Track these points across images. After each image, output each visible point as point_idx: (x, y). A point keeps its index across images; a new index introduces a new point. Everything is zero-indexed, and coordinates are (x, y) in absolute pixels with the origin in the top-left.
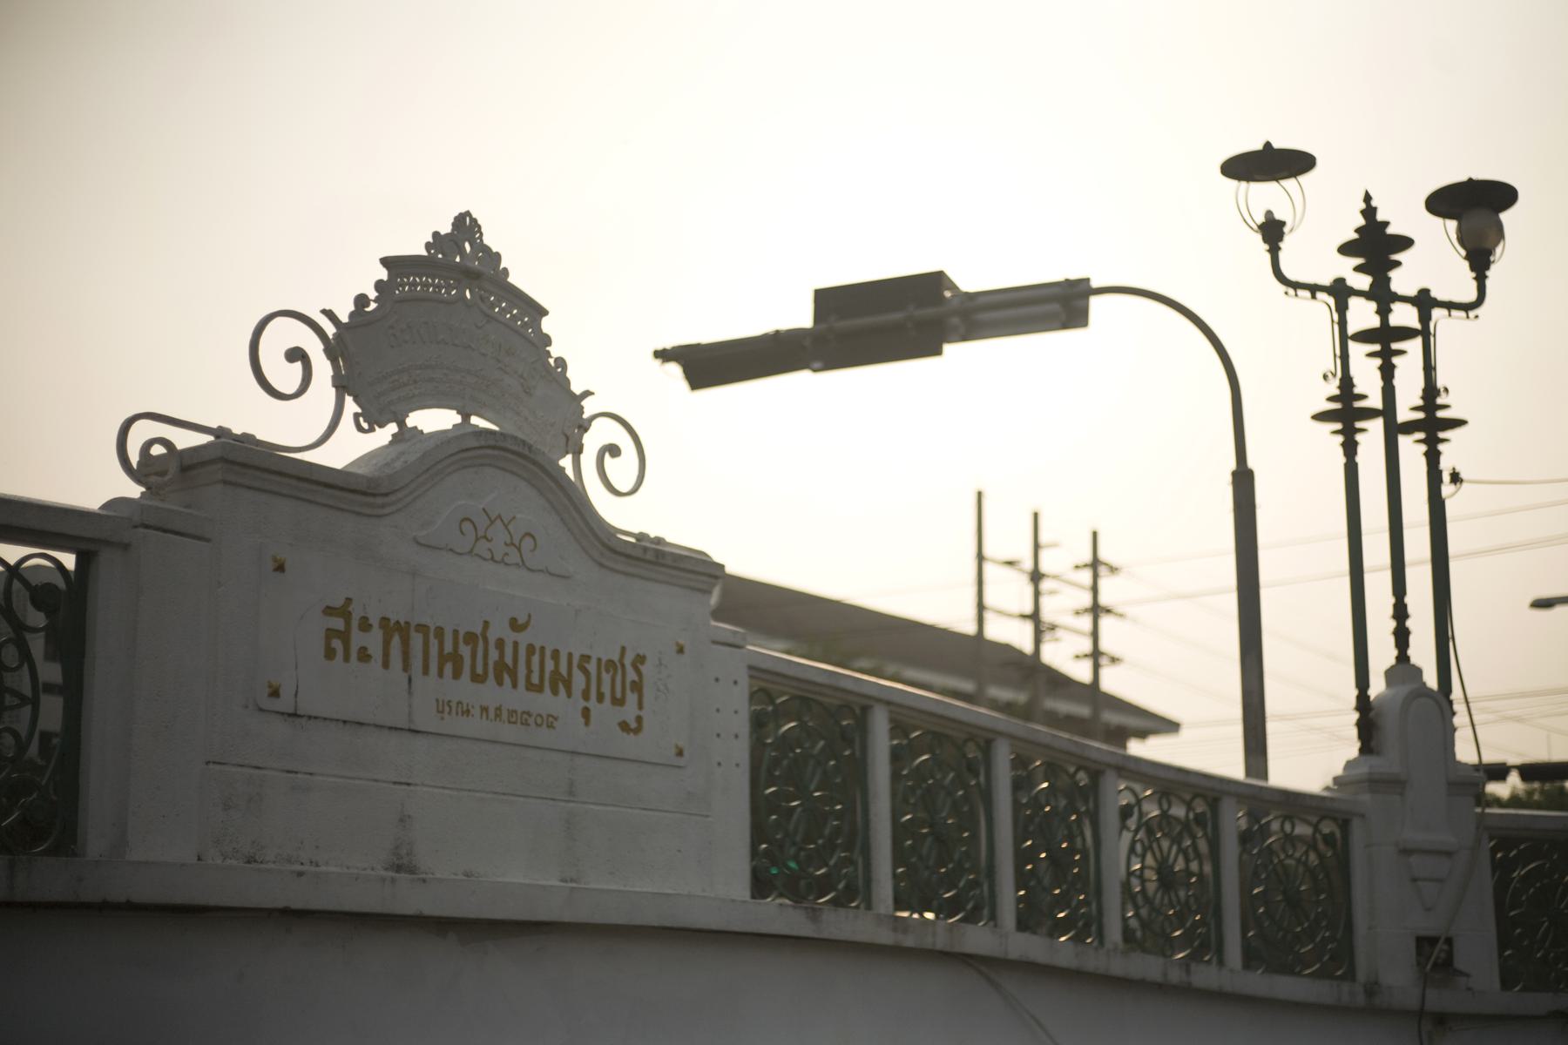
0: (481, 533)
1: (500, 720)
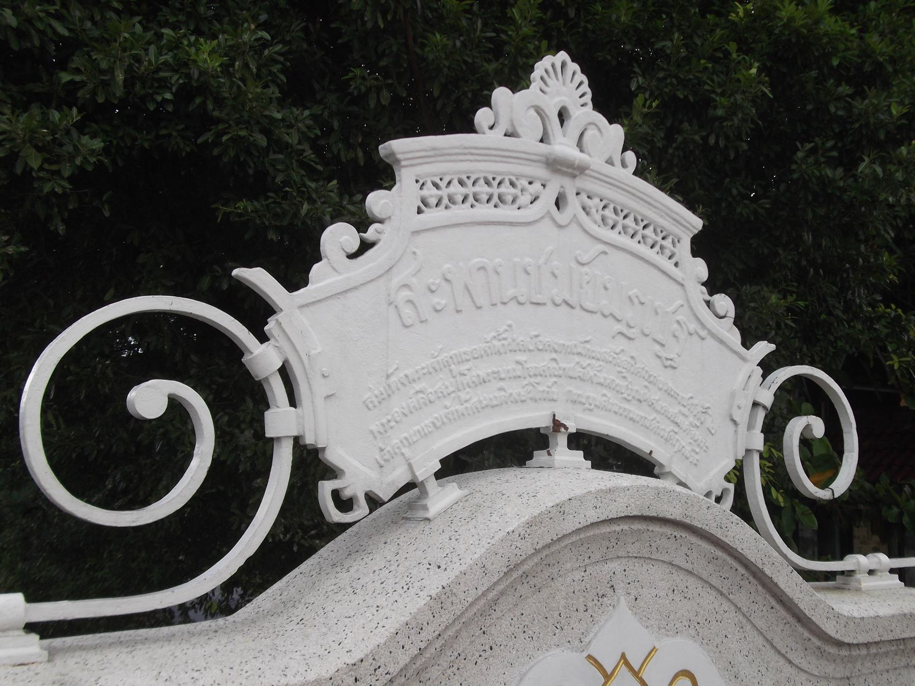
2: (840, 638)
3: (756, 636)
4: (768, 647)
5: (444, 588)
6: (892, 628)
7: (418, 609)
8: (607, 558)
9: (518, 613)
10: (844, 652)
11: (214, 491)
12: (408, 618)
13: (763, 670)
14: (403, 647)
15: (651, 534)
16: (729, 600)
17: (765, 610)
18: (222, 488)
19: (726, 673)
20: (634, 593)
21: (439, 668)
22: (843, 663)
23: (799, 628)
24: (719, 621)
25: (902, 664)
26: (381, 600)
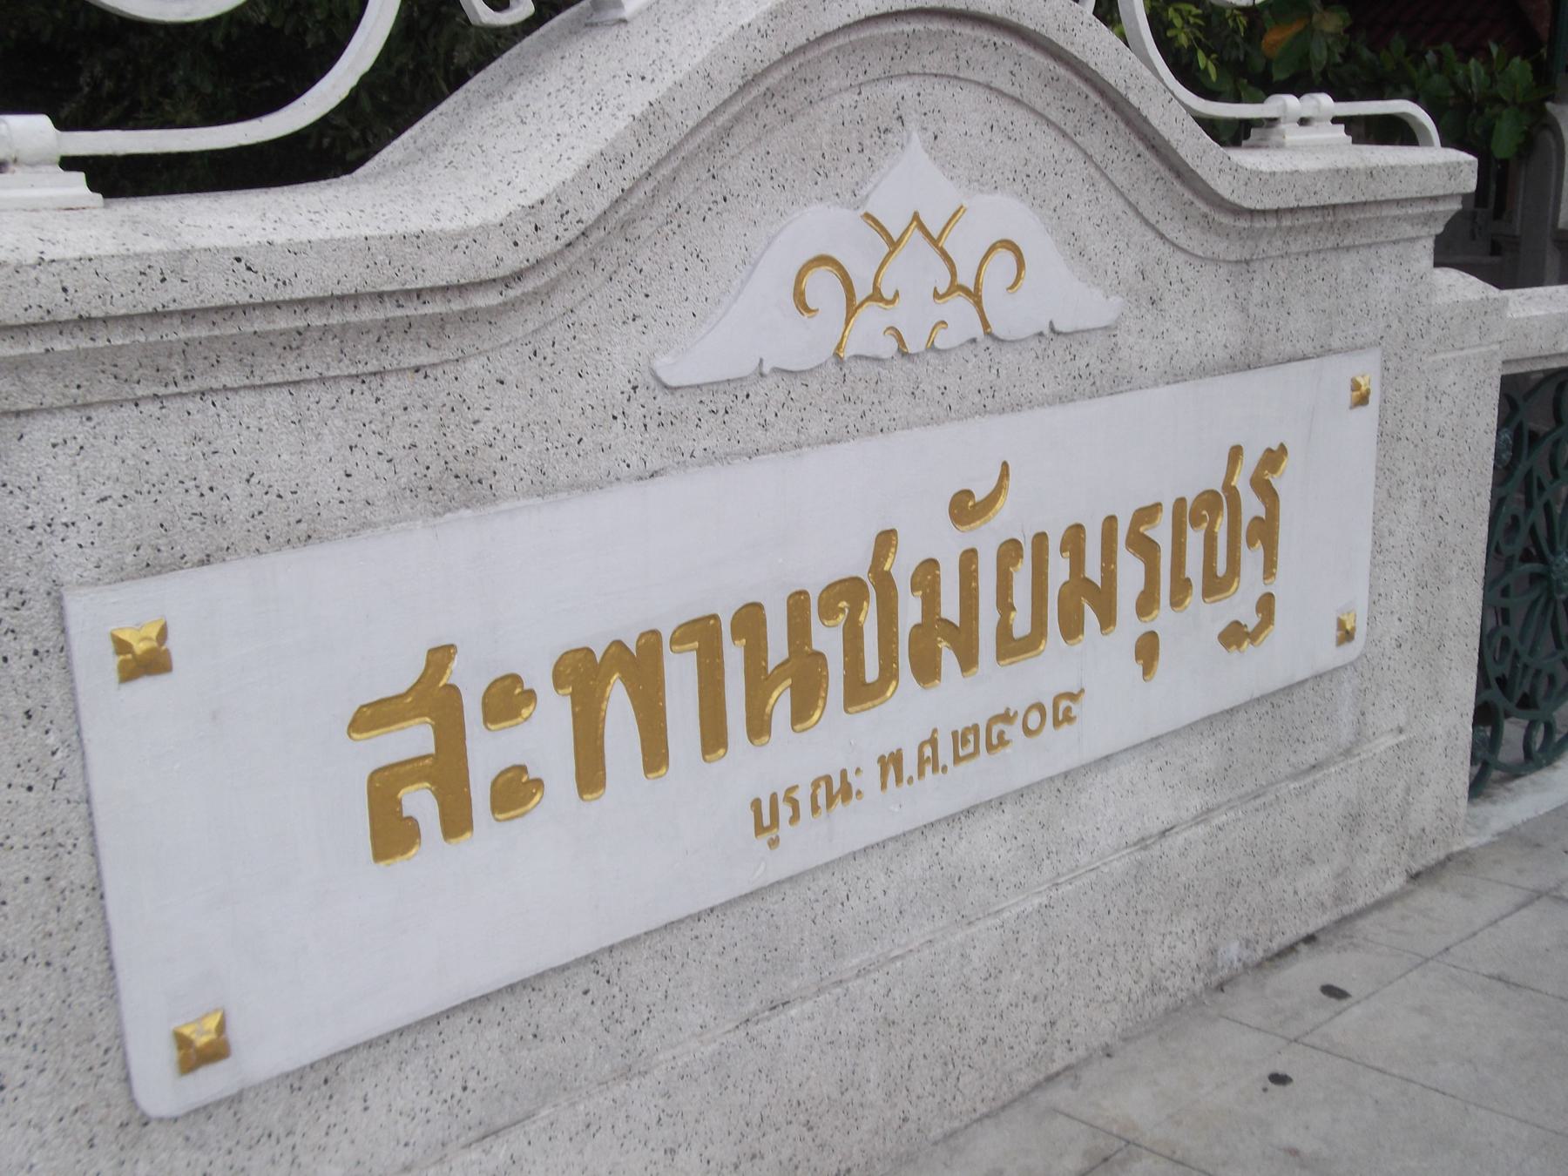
0: (862, 290)
1: (935, 769)
2: (1237, 201)
3: (1114, 197)
4: (1131, 213)
5: (651, 104)
6: (1317, 189)
7: (616, 134)
8: (892, 73)
9: (762, 150)
10: (1243, 223)
11: (268, 83)
12: (602, 146)
13: (1122, 245)
14: (599, 186)
15: (957, 39)
16: (1075, 143)
17: (1128, 159)
18: (282, 80)
19: (1067, 247)
20: (932, 128)
21: (653, 222)
22: (1241, 239)
23: (1178, 186)
24: (1060, 173)
25: (1329, 245)
26: (562, 127)
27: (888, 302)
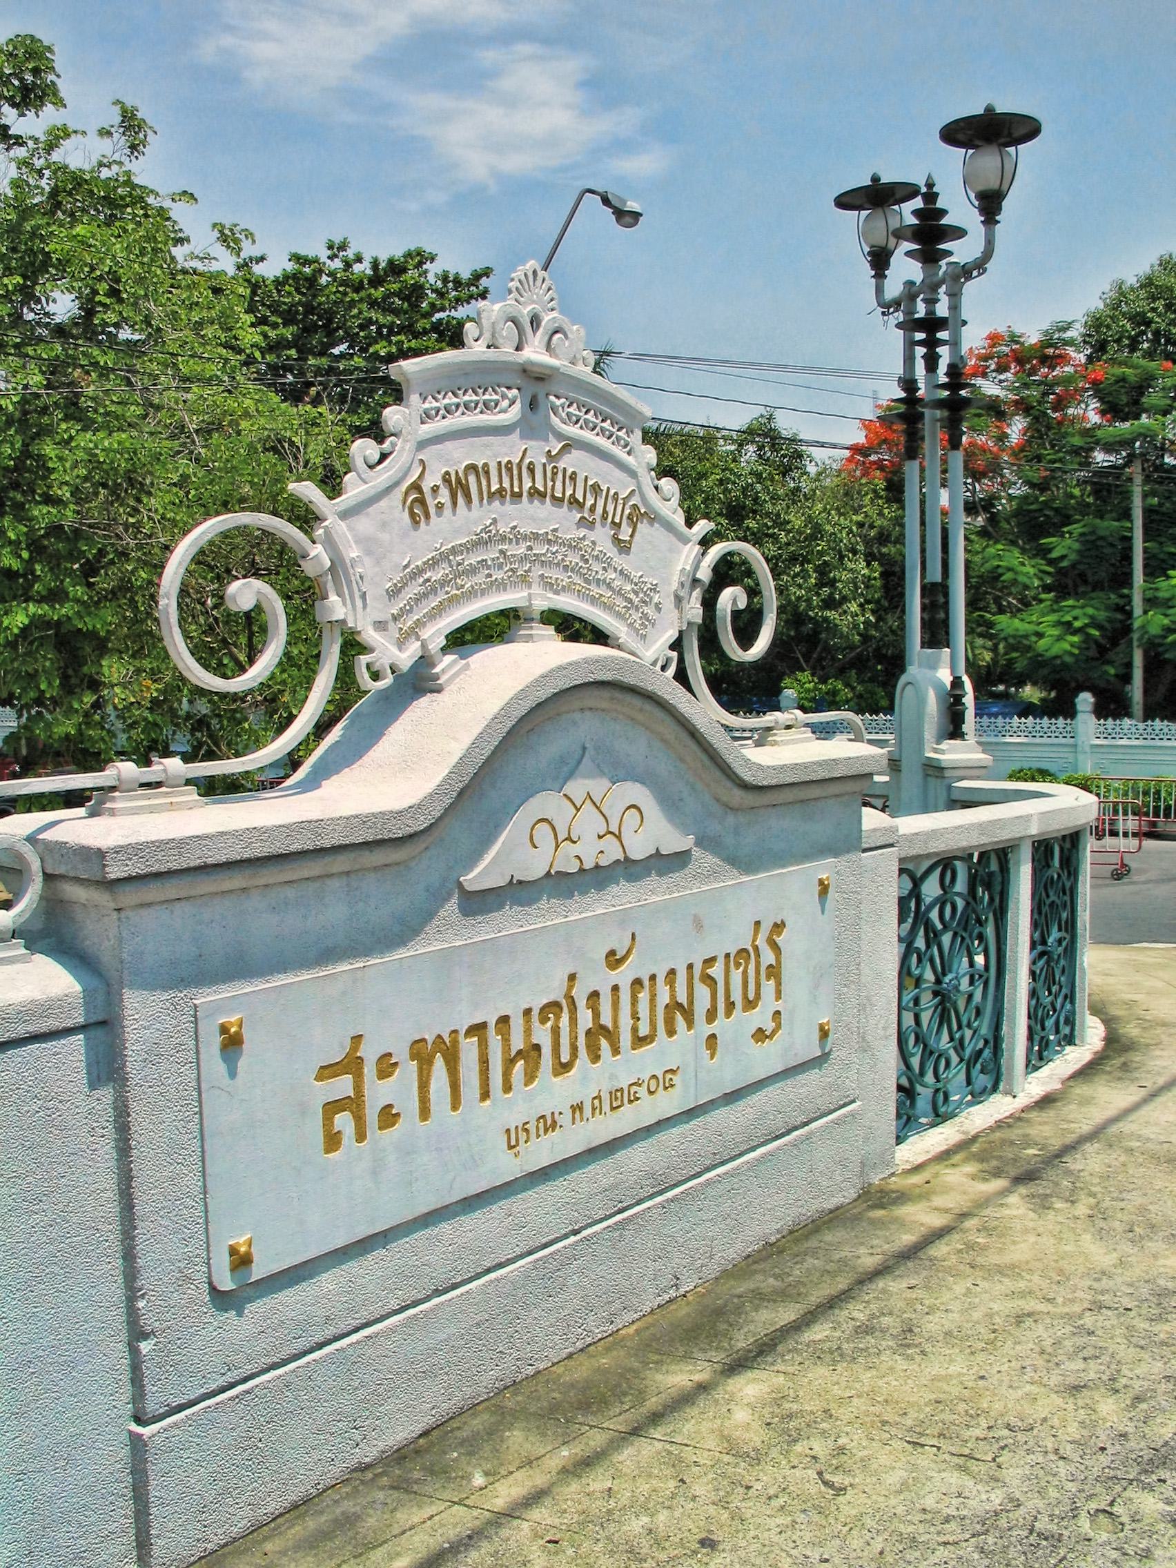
27: (575, 842)
